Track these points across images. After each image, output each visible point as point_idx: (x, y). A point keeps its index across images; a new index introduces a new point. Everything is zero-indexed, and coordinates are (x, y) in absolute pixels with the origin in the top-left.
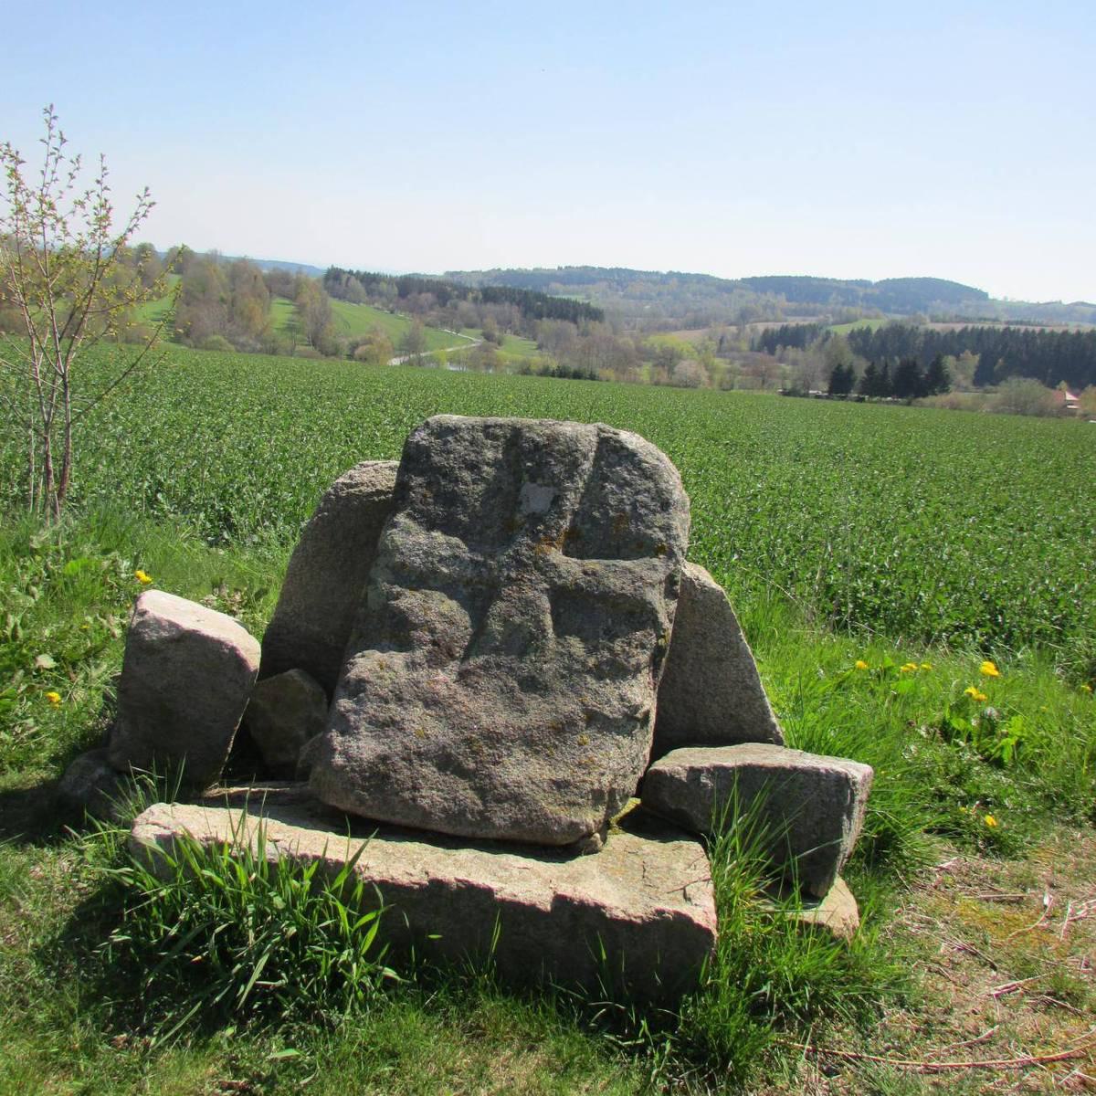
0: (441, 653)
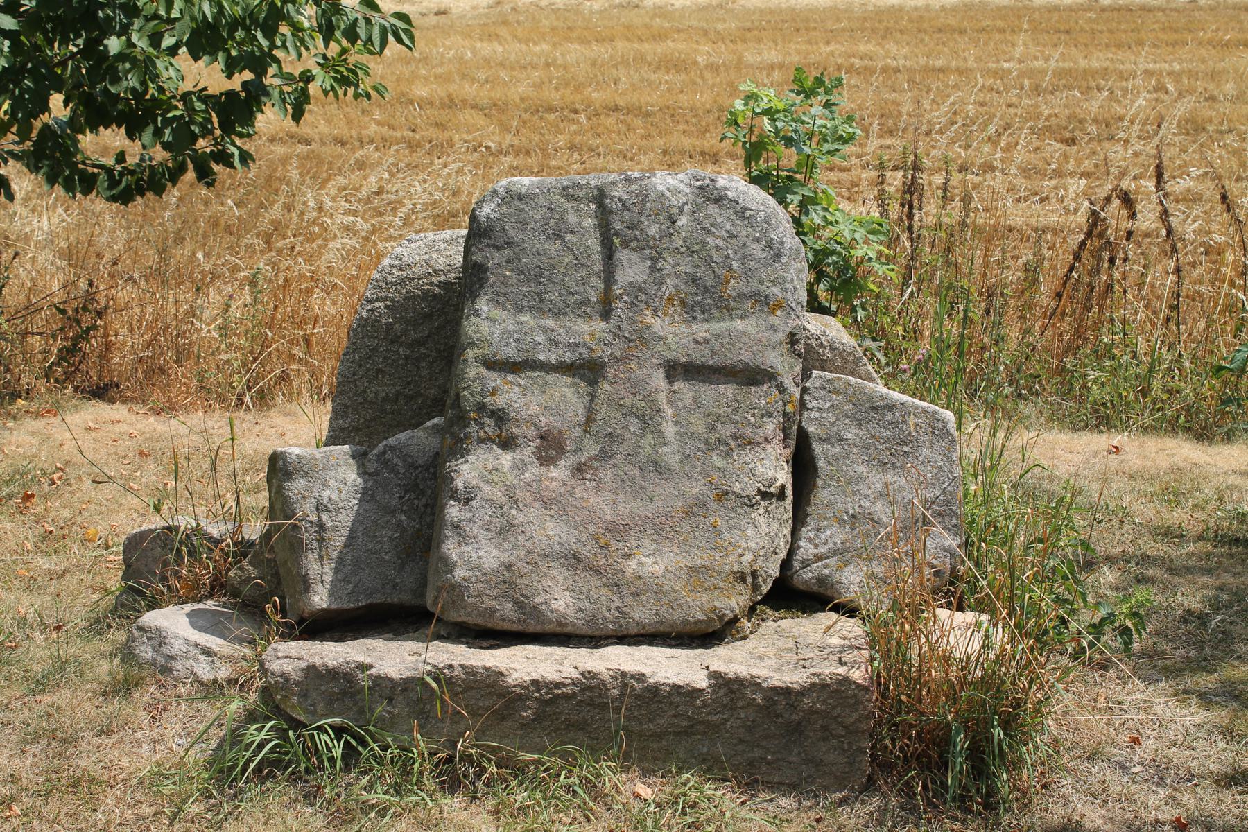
0: (550, 447)
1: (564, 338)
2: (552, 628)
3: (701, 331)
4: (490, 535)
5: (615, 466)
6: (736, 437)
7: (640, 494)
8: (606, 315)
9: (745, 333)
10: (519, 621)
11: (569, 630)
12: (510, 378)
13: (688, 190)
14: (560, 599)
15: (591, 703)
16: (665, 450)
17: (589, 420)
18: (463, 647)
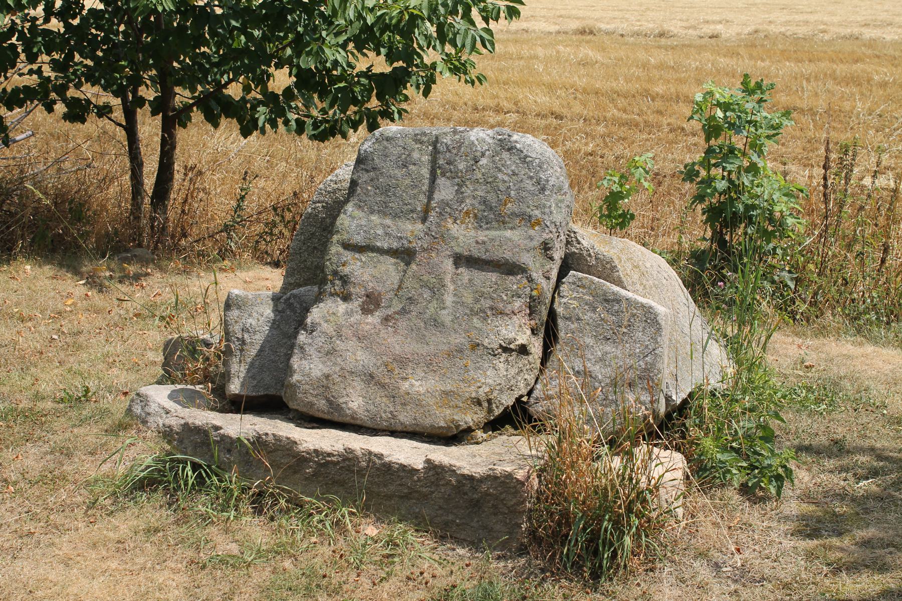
1: (395, 233)
2: (347, 419)
3: (482, 236)
4: (320, 355)
5: (409, 319)
6: (492, 308)
7: (422, 339)
8: (424, 220)
9: (510, 240)
10: (329, 412)
11: (359, 422)
12: (357, 255)
13: (491, 141)
14: (355, 401)
15: (349, 470)
16: (443, 312)
17: (400, 287)
18: (292, 425)
